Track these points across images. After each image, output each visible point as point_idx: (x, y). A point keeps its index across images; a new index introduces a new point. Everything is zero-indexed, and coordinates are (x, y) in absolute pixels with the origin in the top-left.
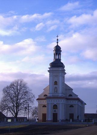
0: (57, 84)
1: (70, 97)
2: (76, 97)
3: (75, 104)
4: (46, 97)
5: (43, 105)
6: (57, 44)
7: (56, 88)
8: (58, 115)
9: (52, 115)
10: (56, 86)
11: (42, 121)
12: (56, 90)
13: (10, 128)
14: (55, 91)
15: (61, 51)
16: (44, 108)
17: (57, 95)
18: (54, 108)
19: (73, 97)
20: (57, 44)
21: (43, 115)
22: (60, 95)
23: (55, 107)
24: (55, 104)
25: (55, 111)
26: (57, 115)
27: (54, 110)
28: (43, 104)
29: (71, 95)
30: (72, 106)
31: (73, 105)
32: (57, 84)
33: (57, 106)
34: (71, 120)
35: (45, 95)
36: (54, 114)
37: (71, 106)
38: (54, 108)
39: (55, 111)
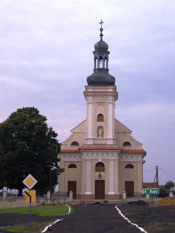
0: (103, 120)
1: (127, 148)
2: (138, 148)
3: (137, 162)
4: (76, 148)
5: (69, 164)
6: (101, 37)
7: (100, 127)
8: (106, 184)
9: (94, 182)
10: (100, 124)
11: (94, 197)
12: (100, 133)
13: (31, 213)
14: (98, 135)
15: (109, 53)
16: (127, 169)
17: (103, 142)
18: (97, 170)
19: (133, 147)
20: (101, 37)
21: (68, 184)
22: (110, 142)
23: (100, 166)
24: (100, 161)
25: (100, 175)
26: (104, 184)
27: (99, 173)
28: (69, 162)
29: (127, 144)
30: (130, 166)
31: (133, 164)
32: (103, 120)
33: (104, 165)
34: (71, 194)
35: (75, 144)
36: (96, 181)
37: (128, 165)
38: (97, 170)
39: (100, 175)
